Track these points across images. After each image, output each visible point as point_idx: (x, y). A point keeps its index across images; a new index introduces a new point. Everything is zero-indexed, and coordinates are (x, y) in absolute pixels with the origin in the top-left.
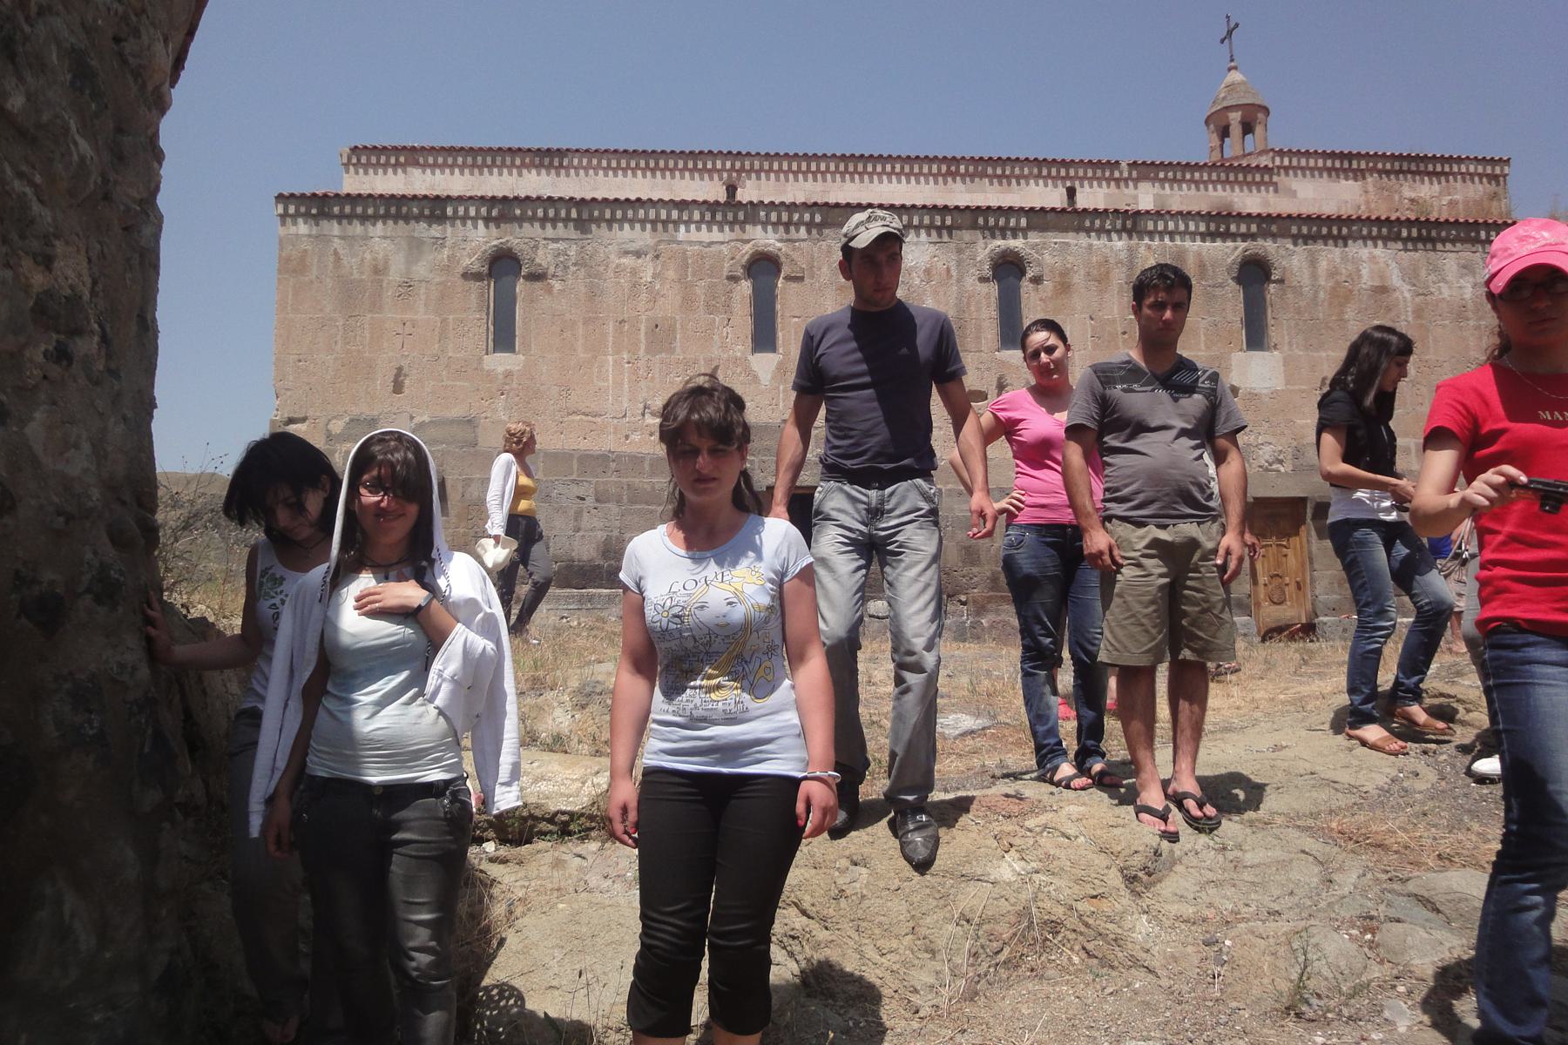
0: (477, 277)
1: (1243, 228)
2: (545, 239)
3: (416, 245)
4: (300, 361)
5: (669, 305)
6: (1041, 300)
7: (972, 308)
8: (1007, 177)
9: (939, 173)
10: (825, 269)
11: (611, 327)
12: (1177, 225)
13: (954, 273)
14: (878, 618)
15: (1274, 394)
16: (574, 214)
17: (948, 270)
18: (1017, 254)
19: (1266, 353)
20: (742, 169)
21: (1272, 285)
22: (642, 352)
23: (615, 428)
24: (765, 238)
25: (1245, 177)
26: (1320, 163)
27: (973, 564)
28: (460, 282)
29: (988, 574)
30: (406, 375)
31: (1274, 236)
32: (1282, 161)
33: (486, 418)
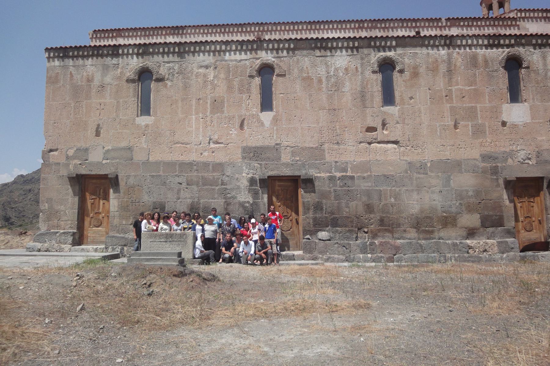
0: (133, 81)
1: (507, 42)
2: (164, 62)
3: (106, 68)
4: (55, 123)
5: (221, 90)
6: (403, 81)
7: (369, 86)
8: (387, 28)
9: (355, 28)
10: (296, 70)
11: (194, 102)
12: (472, 42)
13: (360, 70)
14: (323, 240)
15: (525, 125)
16: (177, 50)
17: (357, 68)
18: (391, 59)
19: (521, 104)
20: (263, 31)
21: (523, 70)
22: (208, 114)
23: (196, 150)
24: (267, 57)
25: (503, 23)
26: (540, 15)
27: (371, 213)
28: (125, 84)
29: (378, 218)
30: (101, 128)
31: (523, 45)
32: (521, 15)
33: (137, 147)
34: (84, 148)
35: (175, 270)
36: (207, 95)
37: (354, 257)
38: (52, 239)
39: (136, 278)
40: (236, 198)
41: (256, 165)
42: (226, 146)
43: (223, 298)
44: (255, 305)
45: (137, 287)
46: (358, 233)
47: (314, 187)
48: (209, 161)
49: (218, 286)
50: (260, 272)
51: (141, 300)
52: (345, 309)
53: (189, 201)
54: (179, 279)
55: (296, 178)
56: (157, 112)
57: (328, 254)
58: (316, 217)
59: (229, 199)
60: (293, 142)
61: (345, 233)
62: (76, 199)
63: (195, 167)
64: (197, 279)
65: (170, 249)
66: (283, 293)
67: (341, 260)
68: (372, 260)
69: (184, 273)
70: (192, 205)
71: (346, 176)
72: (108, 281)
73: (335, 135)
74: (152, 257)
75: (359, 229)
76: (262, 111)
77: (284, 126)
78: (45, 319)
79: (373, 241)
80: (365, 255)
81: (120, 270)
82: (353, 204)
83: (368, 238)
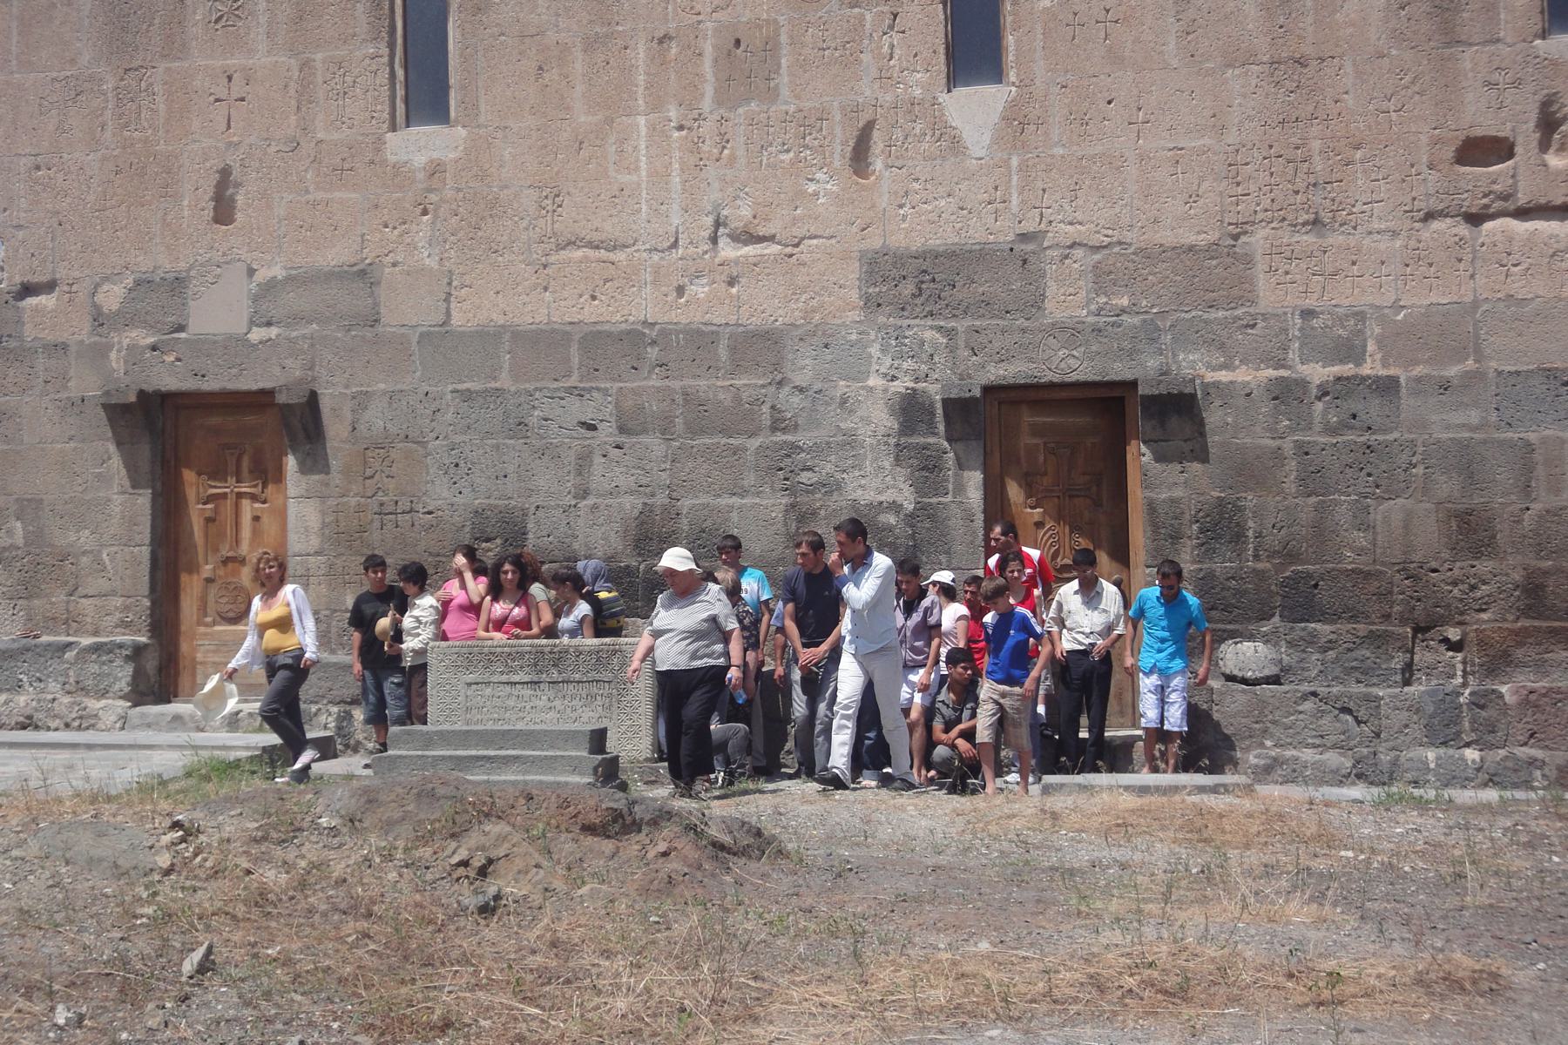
4: (38, 168)
11: (640, 53)
14: (1244, 681)
22: (707, 104)
23: (657, 271)
27: (1478, 555)
29: (1517, 576)
30: (238, 185)
33: (394, 265)
34: (167, 276)
35: (592, 803)
36: (700, 18)
37: (1397, 758)
38: (49, 677)
39: (425, 839)
40: (839, 487)
41: (928, 335)
42: (789, 250)
43: (806, 929)
44: (954, 963)
45: (429, 877)
46: (1417, 649)
47: (1202, 434)
48: (716, 321)
49: (781, 882)
50: (960, 821)
51: (451, 934)
52: (1381, 992)
53: (631, 504)
54: (608, 846)
55: (1117, 393)
56: (476, 106)
57: (1268, 743)
58: (1211, 575)
59: (808, 492)
60: (1102, 222)
61: (1349, 650)
62: (143, 501)
63: (653, 353)
64: (685, 845)
65: (552, 715)
66: (1079, 912)
67: (1332, 771)
68: (1483, 776)
69: (629, 820)
70: (642, 523)
71: (1355, 377)
72: (304, 850)
73: (1301, 185)
74: (481, 753)
75: (1417, 630)
76: (953, 81)
77: (1059, 151)
78: (52, 1009)
79: (1489, 685)
80: (1451, 751)
81: (353, 801)
82: (1390, 512)
83: (1464, 671)
